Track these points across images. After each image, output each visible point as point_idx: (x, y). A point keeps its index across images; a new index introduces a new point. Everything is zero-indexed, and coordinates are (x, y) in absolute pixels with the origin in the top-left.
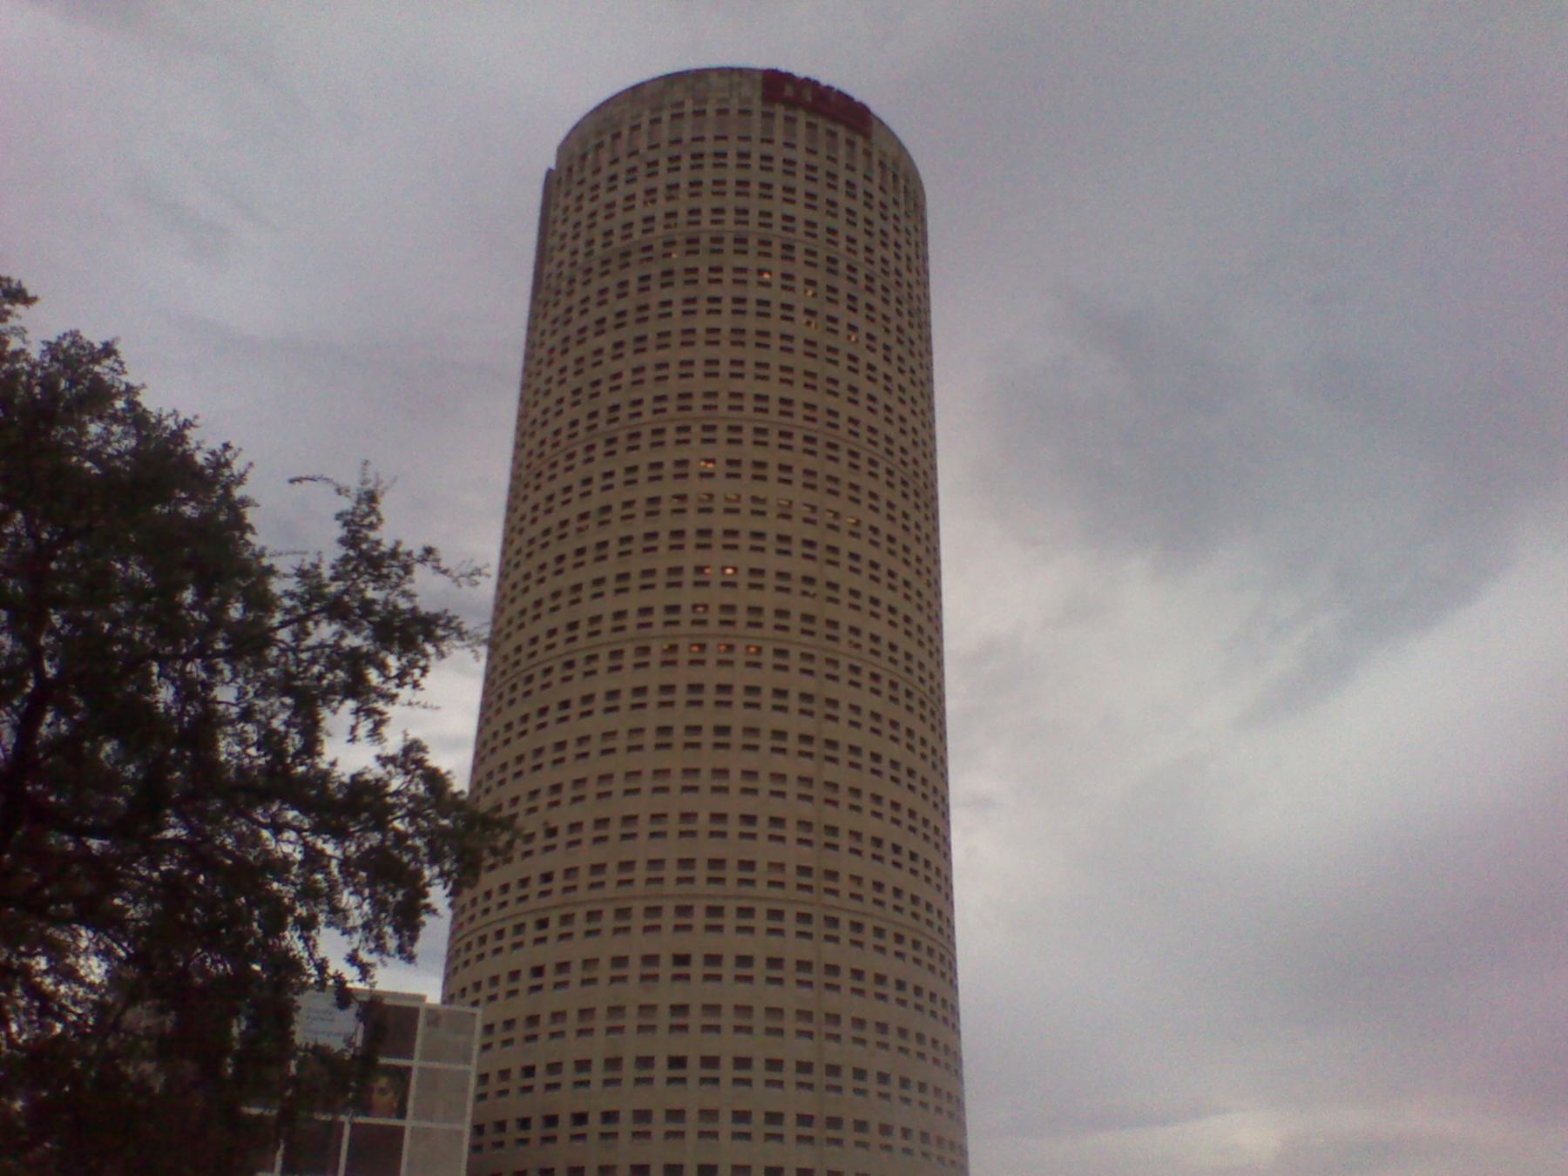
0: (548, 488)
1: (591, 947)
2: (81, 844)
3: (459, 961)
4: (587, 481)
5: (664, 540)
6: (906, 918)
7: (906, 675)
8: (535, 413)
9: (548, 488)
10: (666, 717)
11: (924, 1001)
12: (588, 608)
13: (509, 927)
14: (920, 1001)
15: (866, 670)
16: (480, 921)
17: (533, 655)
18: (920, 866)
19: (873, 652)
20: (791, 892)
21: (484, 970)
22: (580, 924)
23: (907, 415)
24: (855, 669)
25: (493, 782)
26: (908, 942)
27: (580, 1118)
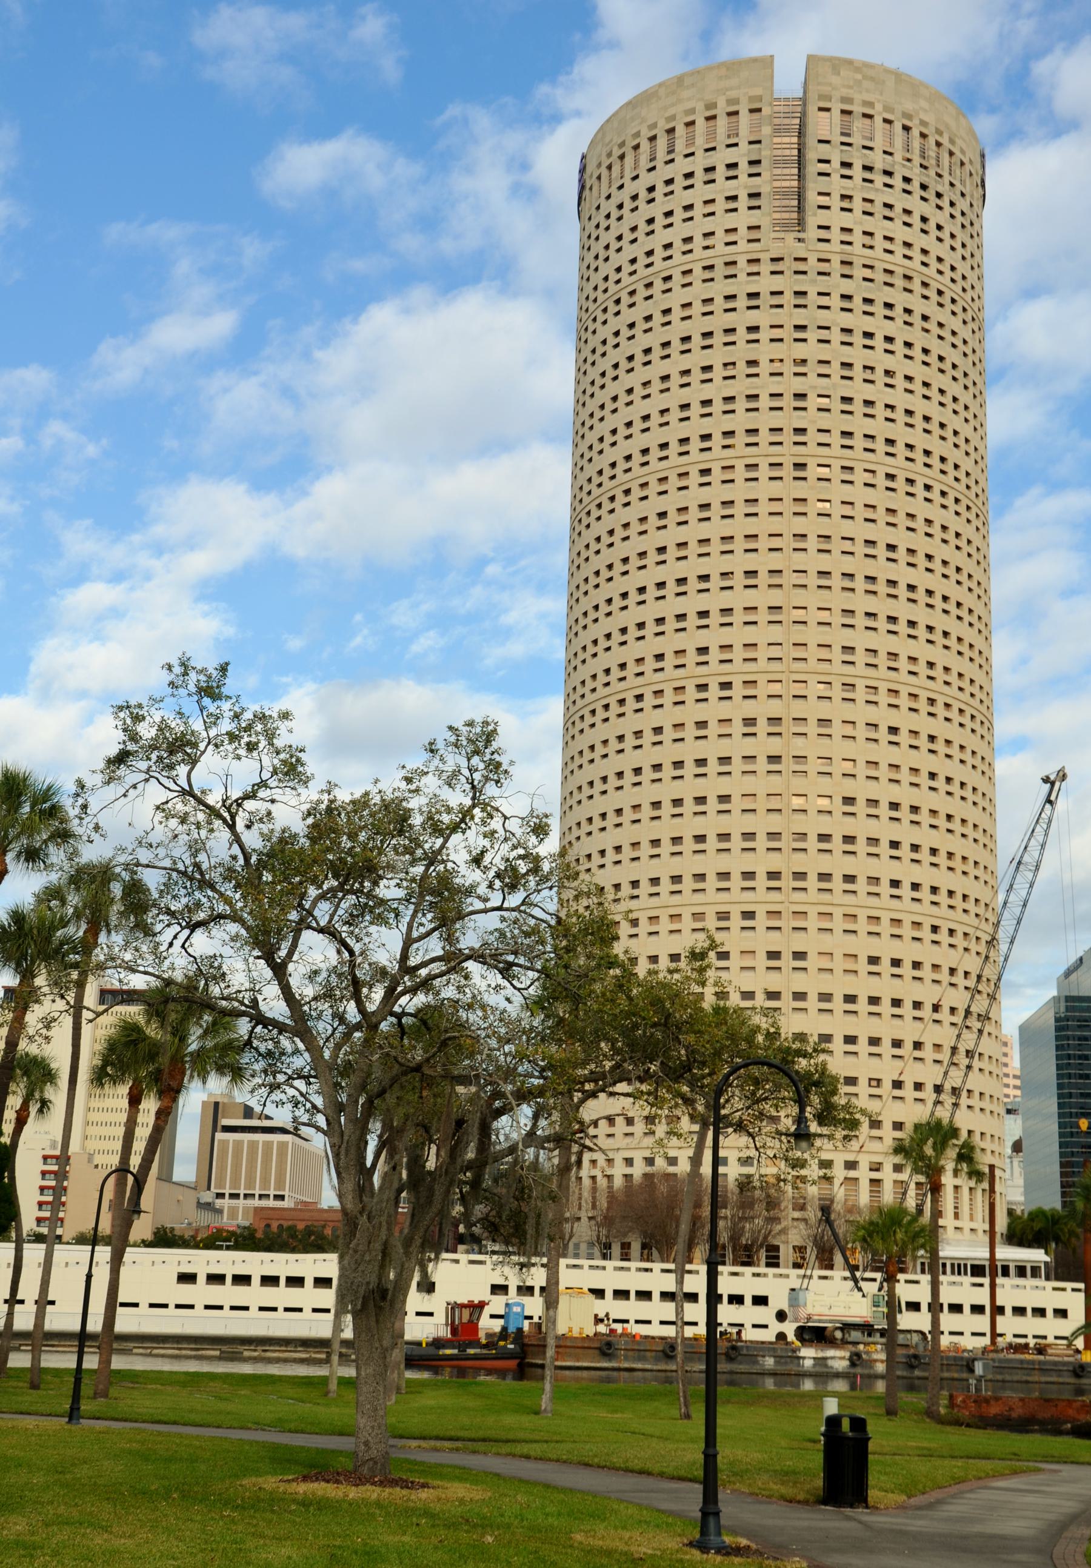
0: (614, 323)
1: (686, 362)
2: (290, 883)
3: (573, 801)
4: (650, 253)
5: (721, 172)
6: (953, 691)
7: (951, 285)
8: (593, 373)
9: (614, 323)
10: (731, 221)
11: (968, 793)
12: (662, 236)
13: (613, 701)
14: (964, 794)
15: (924, 695)
16: (590, 697)
17: (618, 282)
18: (965, 649)
19: (924, 264)
20: (858, 453)
21: (594, 736)
22: (669, 697)
23: (957, 231)
24: (910, 482)
25: (589, 587)
26: (960, 935)
27: (676, 879)
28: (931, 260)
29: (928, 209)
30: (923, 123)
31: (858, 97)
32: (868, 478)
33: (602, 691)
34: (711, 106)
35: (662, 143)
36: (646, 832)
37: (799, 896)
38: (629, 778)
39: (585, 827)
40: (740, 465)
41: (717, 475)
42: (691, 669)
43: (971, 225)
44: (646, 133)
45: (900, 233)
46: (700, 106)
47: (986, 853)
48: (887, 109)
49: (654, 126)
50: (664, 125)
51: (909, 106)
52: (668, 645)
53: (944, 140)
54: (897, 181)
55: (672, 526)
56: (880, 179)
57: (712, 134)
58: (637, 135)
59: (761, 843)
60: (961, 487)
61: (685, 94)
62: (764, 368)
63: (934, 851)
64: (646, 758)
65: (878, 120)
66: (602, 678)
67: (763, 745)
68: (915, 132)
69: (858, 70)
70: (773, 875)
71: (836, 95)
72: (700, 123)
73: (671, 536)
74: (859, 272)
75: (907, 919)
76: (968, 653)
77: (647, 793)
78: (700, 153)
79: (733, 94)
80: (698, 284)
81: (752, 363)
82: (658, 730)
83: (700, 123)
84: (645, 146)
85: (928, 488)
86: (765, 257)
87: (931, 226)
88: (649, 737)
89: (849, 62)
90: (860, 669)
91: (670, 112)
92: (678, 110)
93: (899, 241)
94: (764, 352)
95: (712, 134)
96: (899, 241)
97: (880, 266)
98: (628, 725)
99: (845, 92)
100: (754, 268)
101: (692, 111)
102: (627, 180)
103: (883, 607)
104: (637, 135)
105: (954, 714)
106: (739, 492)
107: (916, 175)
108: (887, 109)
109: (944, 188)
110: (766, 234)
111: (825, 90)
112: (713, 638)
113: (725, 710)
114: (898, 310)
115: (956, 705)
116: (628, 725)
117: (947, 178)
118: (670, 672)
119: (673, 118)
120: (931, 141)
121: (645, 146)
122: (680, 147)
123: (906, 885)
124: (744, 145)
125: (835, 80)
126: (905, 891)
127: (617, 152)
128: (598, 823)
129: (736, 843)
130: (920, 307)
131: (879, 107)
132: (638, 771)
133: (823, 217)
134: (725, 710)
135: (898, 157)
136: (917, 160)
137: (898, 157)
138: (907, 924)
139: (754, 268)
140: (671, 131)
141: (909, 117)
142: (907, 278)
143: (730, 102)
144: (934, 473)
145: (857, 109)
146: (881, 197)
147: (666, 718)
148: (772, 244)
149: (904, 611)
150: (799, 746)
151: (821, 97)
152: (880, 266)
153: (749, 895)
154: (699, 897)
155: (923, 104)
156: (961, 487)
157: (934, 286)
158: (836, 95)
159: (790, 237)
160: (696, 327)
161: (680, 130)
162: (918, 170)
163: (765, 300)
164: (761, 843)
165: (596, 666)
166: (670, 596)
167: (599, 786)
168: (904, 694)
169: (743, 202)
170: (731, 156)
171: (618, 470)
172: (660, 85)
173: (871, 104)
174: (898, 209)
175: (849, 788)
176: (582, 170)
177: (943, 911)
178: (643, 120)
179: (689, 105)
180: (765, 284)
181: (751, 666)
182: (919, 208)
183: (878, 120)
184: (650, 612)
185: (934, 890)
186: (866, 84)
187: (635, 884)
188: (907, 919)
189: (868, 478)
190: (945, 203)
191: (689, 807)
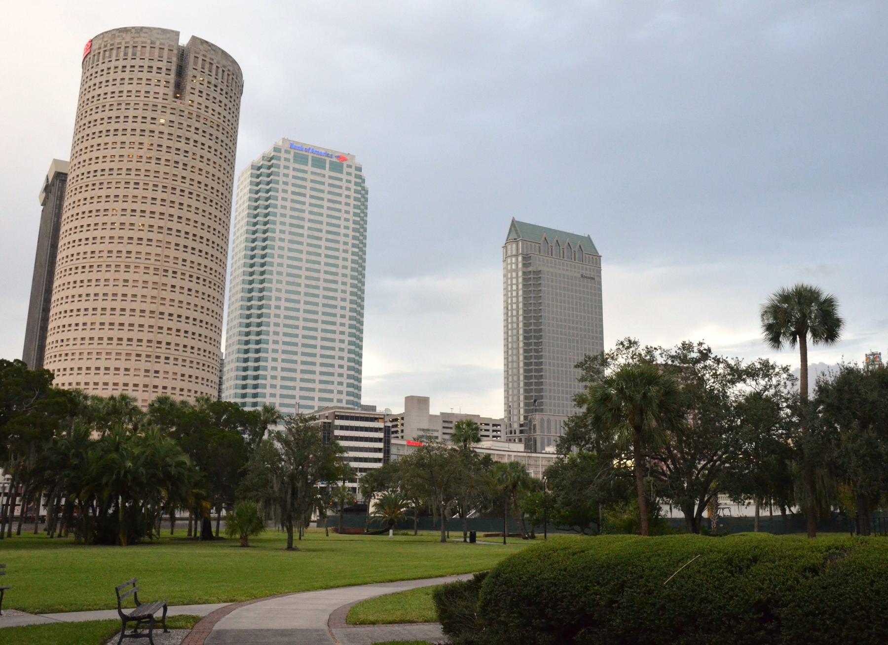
6: (207, 274)
28: (226, 120)
31: (209, 56)
35: (130, 51)
40: (151, 184)
41: (141, 186)
45: (218, 109)
54: (218, 89)
56: (213, 88)
60: (223, 201)
71: (201, 53)
74: (202, 121)
78: (138, 59)
85: (205, 198)
87: (227, 108)
89: (207, 42)
90: (188, 268)
97: (210, 120)
99: (204, 53)
100: (164, 110)
103: (198, 246)
104: (120, 43)
105: (212, 285)
107: (224, 88)
108: (218, 63)
109: (232, 95)
111: (198, 50)
112: (134, 248)
114: (214, 137)
115: (208, 280)
125: (201, 47)
126: (188, 349)
127: (109, 47)
129: (136, 328)
130: (221, 137)
131: (215, 61)
133: (192, 97)
137: (220, 81)
139: (164, 110)
144: (208, 193)
145: (208, 60)
146: (212, 95)
149: (205, 248)
153: (139, 348)
154: (119, 347)
156: (223, 201)
172: (133, 28)
177: (201, 357)
178: (123, 39)
181: (148, 261)
182: (225, 101)
186: (212, 52)
190: (224, 93)
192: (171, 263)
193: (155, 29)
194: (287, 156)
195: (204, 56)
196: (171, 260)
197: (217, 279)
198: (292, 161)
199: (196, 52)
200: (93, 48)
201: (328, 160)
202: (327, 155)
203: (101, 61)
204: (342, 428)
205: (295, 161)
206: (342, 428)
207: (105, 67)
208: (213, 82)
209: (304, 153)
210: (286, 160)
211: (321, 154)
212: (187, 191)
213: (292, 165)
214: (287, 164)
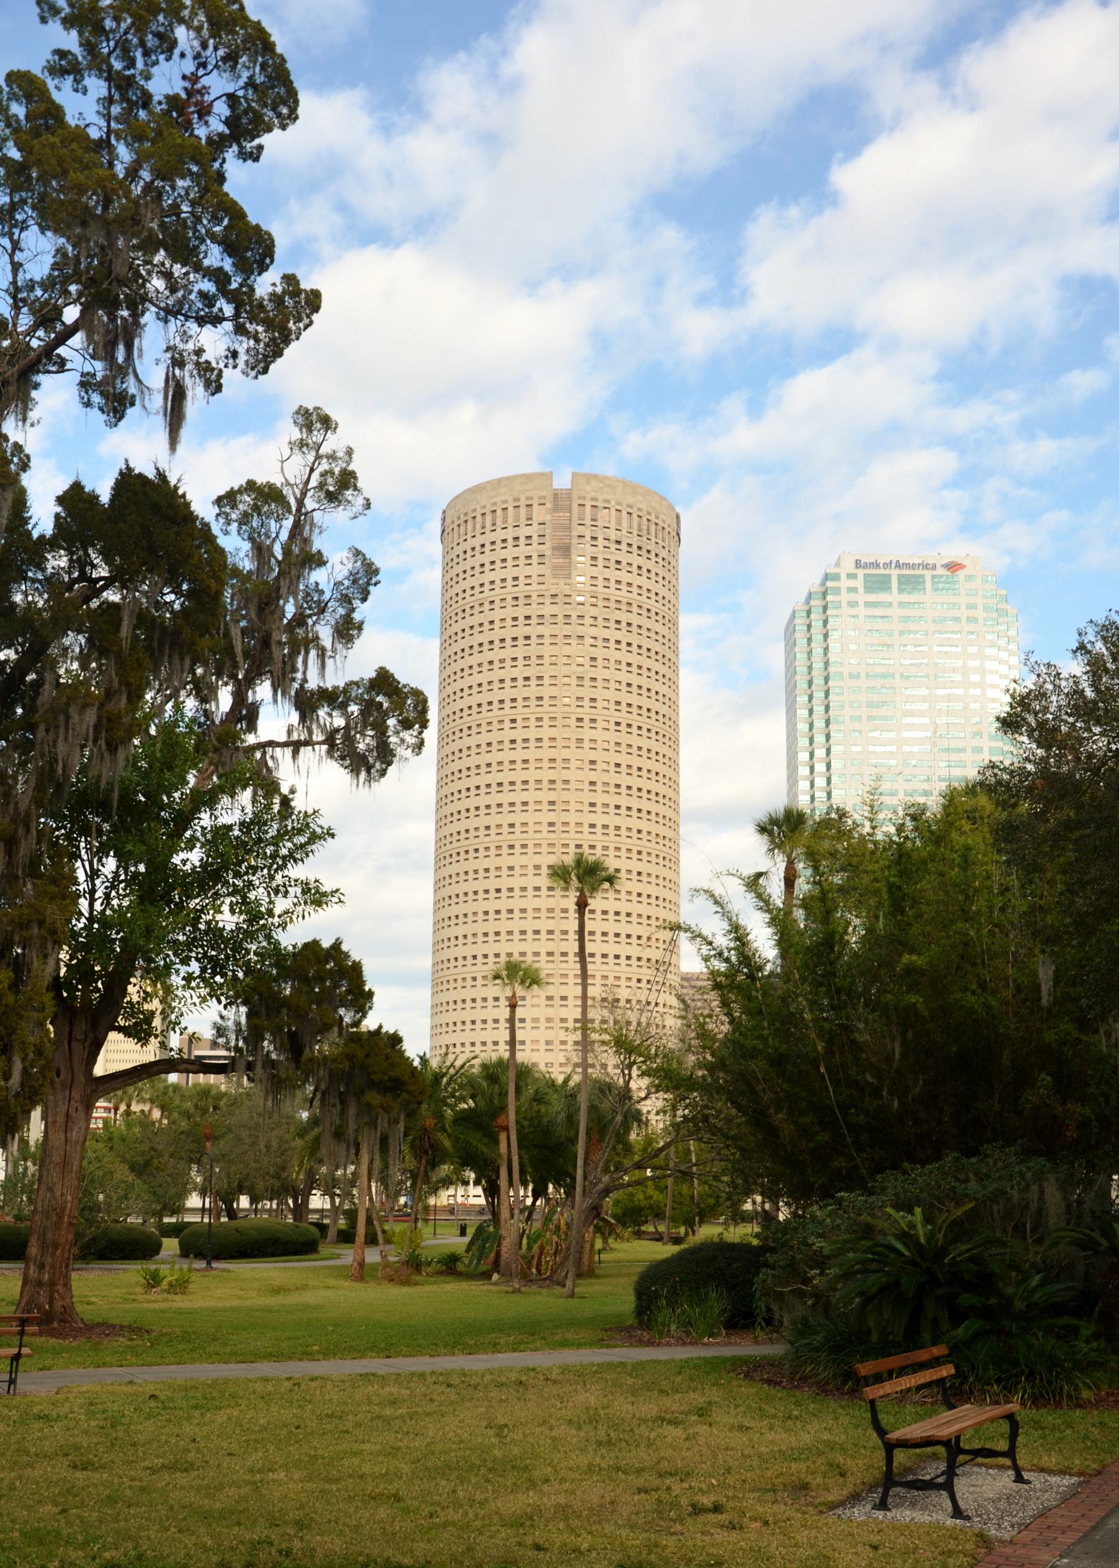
13: (465, 727)
29: (641, 561)
30: (640, 509)
31: (601, 498)
32: (605, 724)
33: (461, 602)
34: (517, 500)
36: (481, 927)
37: (564, 965)
38: (473, 791)
39: (451, 757)
40: (533, 718)
41: (520, 723)
42: (510, 589)
43: (669, 564)
44: (480, 511)
46: (510, 500)
47: (671, 851)
48: (618, 503)
49: (484, 507)
50: (489, 508)
51: (630, 500)
52: (493, 820)
53: (653, 518)
55: (494, 751)
57: (517, 517)
58: (474, 510)
59: (544, 914)
61: (502, 490)
62: (547, 660)
63: (640, 790)
64: (480, 885)
65: (613, 510)
66: (461, 595)
67: (545, 796)
68: (635, 516)
69: (601, 481)
70: (550, 932)
71: (588, 497)
72: (511, 510)
73: (494, 757)
75: (623, 976)
76: (661, 640)
77: (487, 656)
78: (510, 528)
79: (529, 494)
80: (509, 607)
81: (540, 657)
82: (491, 663)
83: (511, 510)
84: (479, 519)
86: (548, 594)
88: (486, 667)
89: (596, 476)
91: (494, 500)
92: (498, 499)
93: (624, 583)
94: (547, 650)
95: (517, 517)
96: (624, 583)
98: (470, 866)
99: (593, 494)
101: (506, 502)
102: (469, 537)
104: (474, 510)
106: (532, 734)
107: (635, 542)
110: (549, 580)
113: (524, 860)
115: (654, 853)
116: (474, 661)
117: (654, 540)
118: (493, 837)
119: (494, 504)
120: (644, 519)
121: (479, 519)
122: (499, 522)
123: (623, 914)
124: (535, 525)
125: (588, 487)
127: (463, 518)
128: (459, 694)
131: (613, 503)
132: (479, 705)
134: (524, 860)
135: (624, 532)
136: (635, 532)
137: (624, 532)
138: (623, 979)
140: (494, 511)
141: (631, 507)
142: (629, 604)
143: (528, 498)
145: (601, 504)
147: (494, 737)
148: (550, 587)
150: (566, 753)
151: (580, 498)
152: (613, 598)
154: (511, 836)
155: (640, 498)
157: (645, 606)
158: (588, 497)
159: (562, 582)
160: (508, 634)
161: (499, 512)
162: (636, 538)
163: (548, 620)
164: (544, 914)
165: (458, 589)
166: (496, 649)
167: (459, 694)
168: (624, 850)
169: (535, 560)
170: (528, 531)
171: (467, 594)
173: (608, 501)
174: (624, 563)
175: (594, 652)
176: (444, 520)
179: (504, 498)
180: (548, 610)
181: (538, 835)
182: (636, 560)
183: (613, 510)
184: (482, 801)
185: (639, 811)
187: (477, 808)
188: (623, 976)
189: (605, 724)
191: (506, 787)
192: (572, 833)
193: (516, 477)
194: (852, 583)
195: (594, 499)
196: (572, 828)
197: (666, 849)
198: (861, 590)
199: (580, 498)
200: (448, 521)
201: (928, 574)
202: (926, 566)
203: (470, 535)
204: (508, 1138)
205: (869, 589)
206: (508, 1138)
207: (477, 542)
208: (613, 538)
209: (882, 571)
210: (852, 590)
211: (913, 566)
212: (587, 719)
213: (862, 597)
214: (852, 597)
